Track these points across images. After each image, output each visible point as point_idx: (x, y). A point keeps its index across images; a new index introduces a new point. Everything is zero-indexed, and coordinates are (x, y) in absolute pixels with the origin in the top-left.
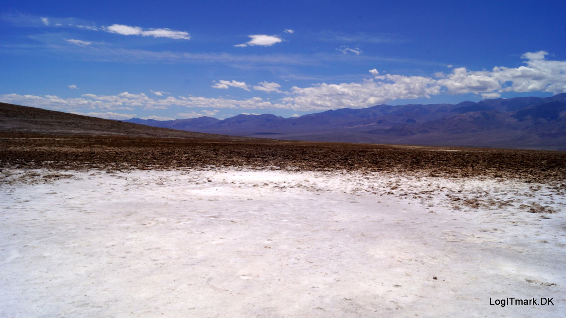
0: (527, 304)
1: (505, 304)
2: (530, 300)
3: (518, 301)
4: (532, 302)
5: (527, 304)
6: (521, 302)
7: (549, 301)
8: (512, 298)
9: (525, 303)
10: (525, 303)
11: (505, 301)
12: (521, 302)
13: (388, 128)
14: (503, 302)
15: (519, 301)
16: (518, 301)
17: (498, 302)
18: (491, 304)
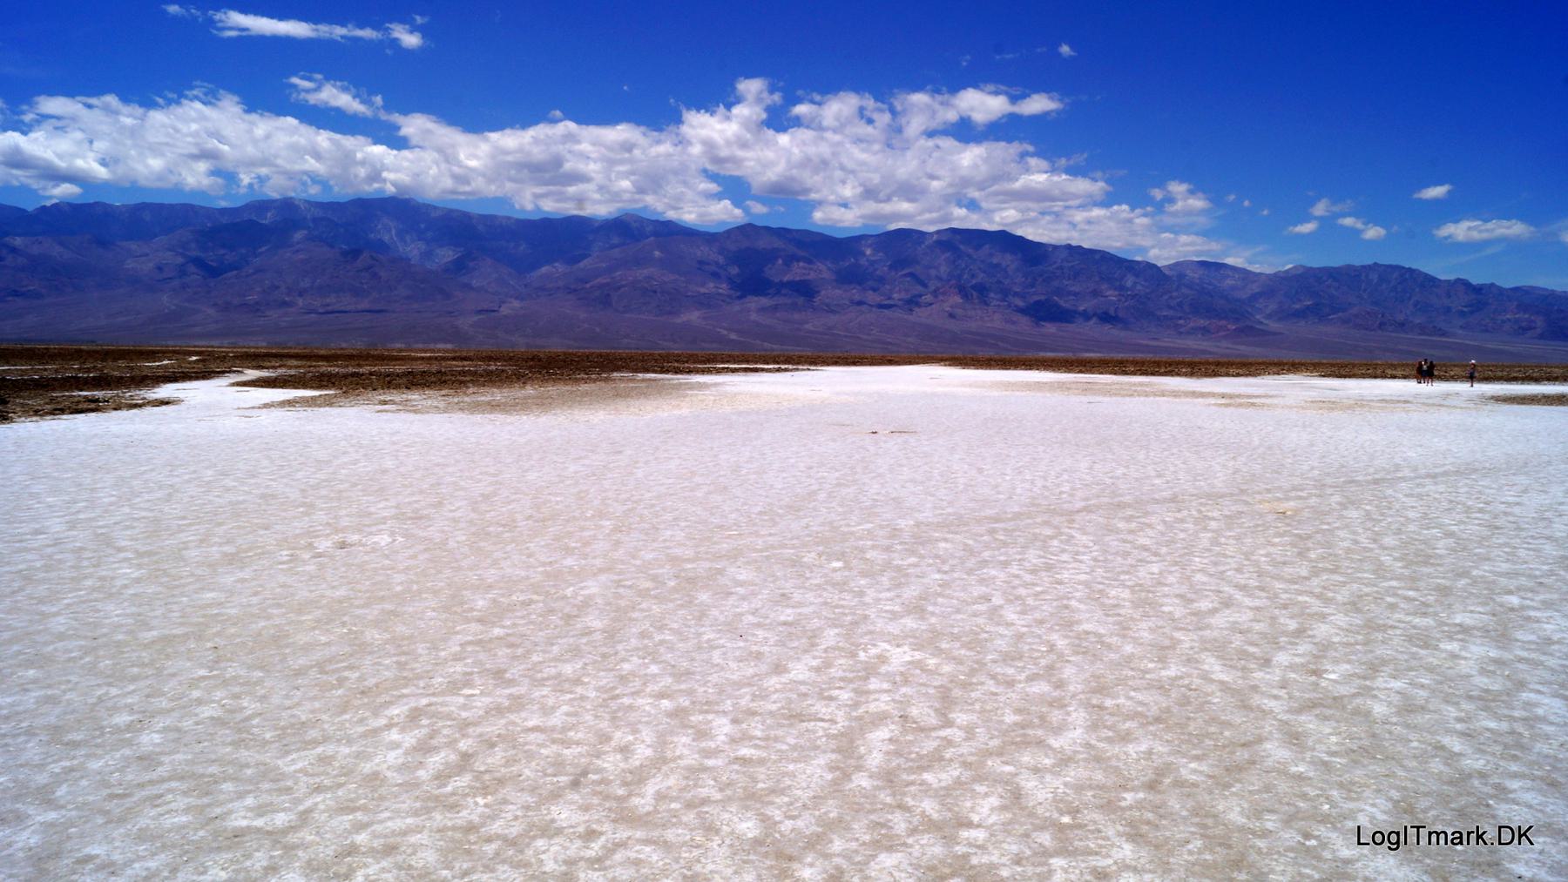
0: (1461, 843)
1: (1398, 843)
2: (1469, 833)
3: (1434, 837)
4: (1473, 836)
5: (1461, 843)
6: (1442, 836)
7: (1520, 836)
8: (1418, 828)
9: (1456, 841)
10: (1456, 841)
11: (1398, 834)
12: (1442, 836)
13: (1039, 50)
14: (1394, 838)
15: (1438, 834)
16: (1434, 837)
17: (1378, 838)
18: (1359, 843)
